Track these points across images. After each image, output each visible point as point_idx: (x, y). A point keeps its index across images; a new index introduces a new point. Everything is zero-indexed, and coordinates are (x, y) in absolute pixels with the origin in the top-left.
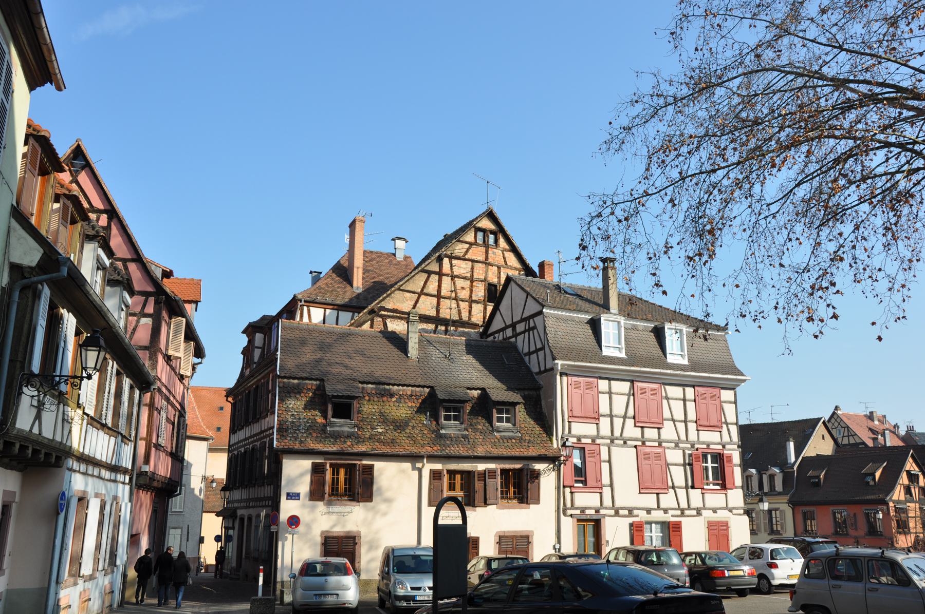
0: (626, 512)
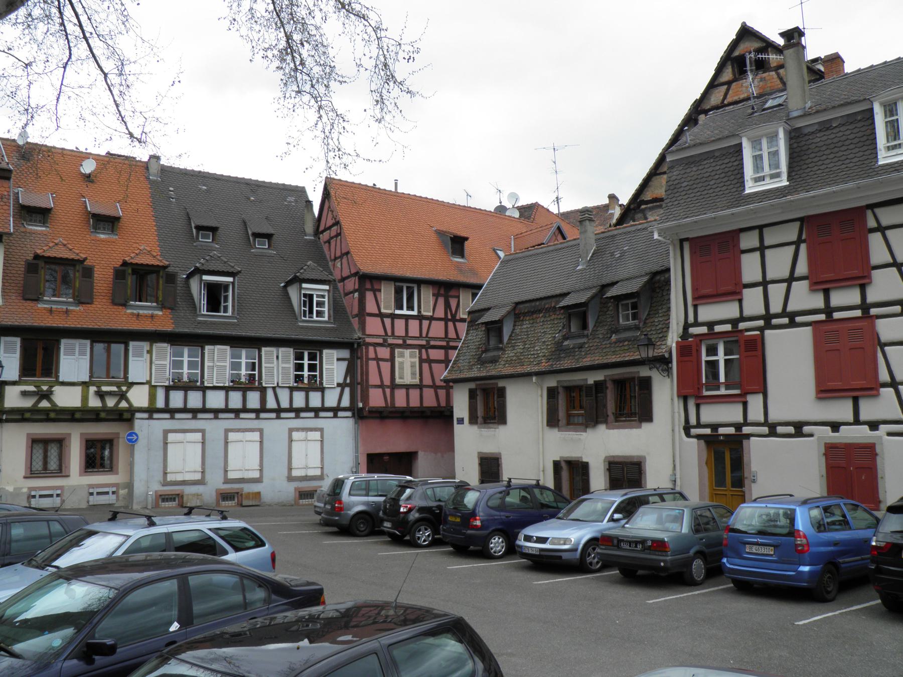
0: (780, 429)
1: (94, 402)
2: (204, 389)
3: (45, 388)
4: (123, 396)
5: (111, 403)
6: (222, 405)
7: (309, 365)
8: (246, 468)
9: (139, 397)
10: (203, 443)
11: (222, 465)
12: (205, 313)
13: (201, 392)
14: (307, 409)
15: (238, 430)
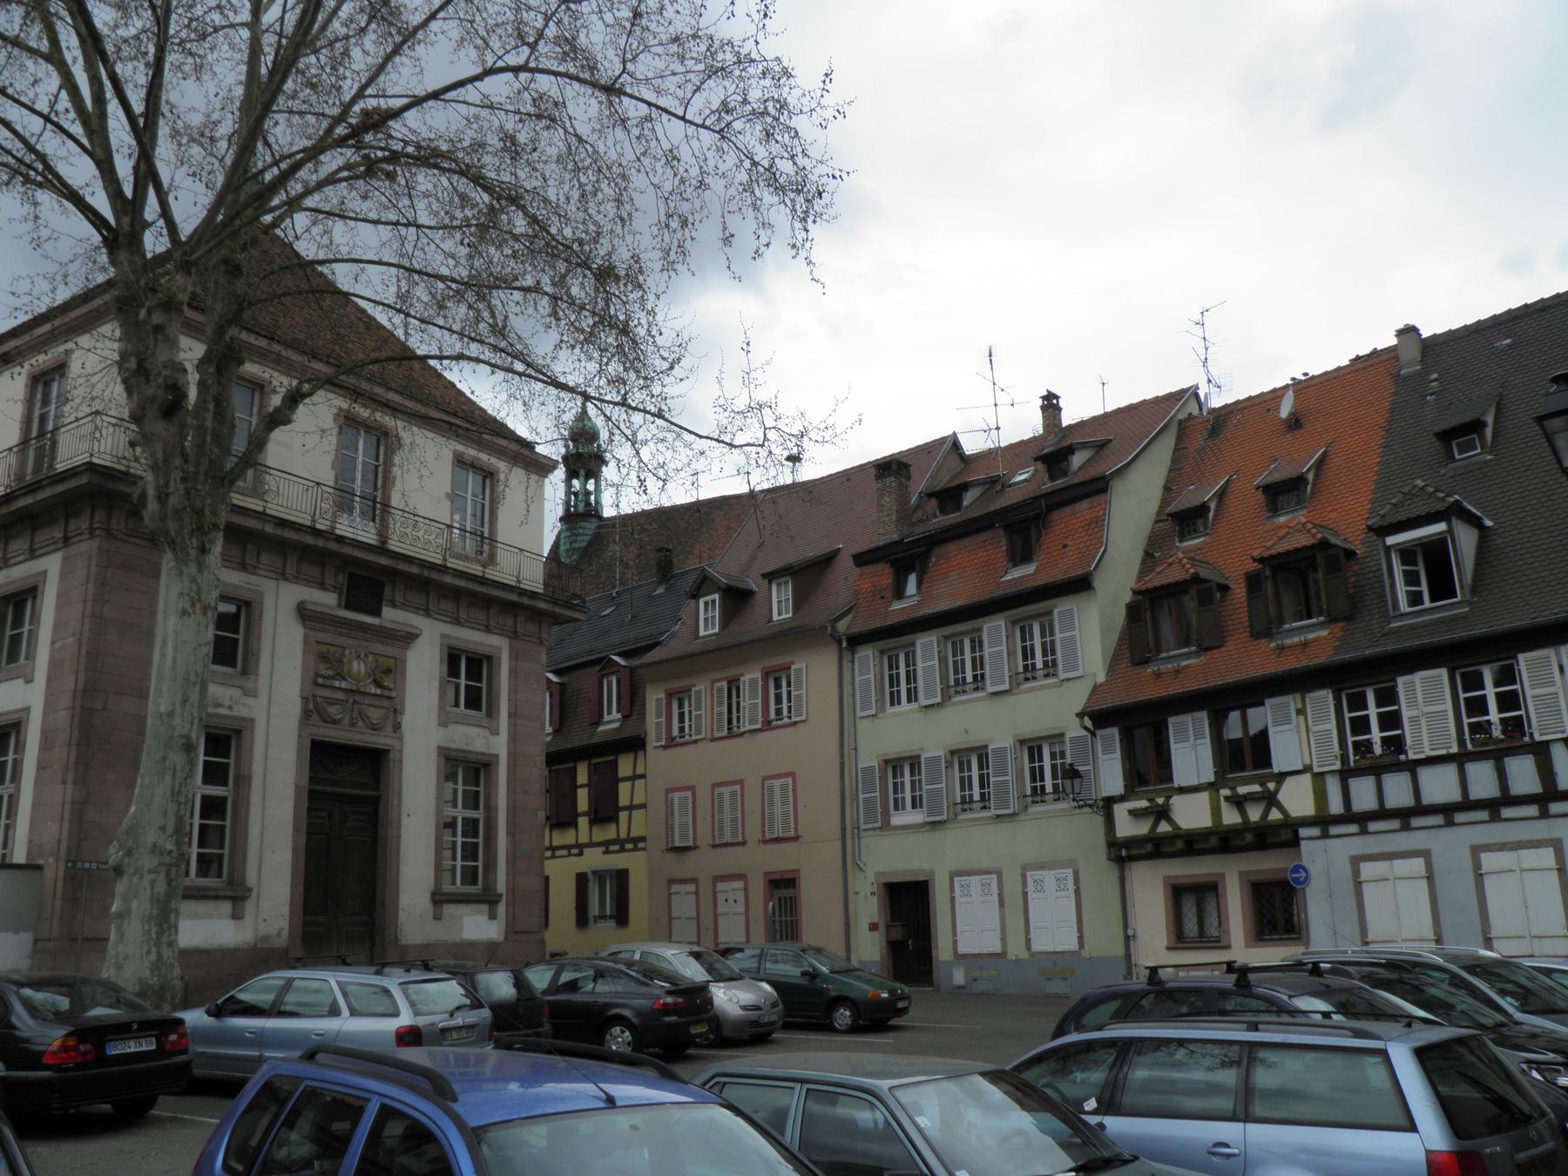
1: (1231, 817)
2: (1412, 767)
3: (1160, 801)
4: (1270, 800)
5: (1255, 814)
6: (1455, 796)
7: (1499, 696)
8: (1535, 932)
9: (1297, 799)
10: (1430, 878)
11: (1478, 927)
12: (1408, 610)
13: (1408, 774)
14: (1382, 814)
15: (1502, 847)
